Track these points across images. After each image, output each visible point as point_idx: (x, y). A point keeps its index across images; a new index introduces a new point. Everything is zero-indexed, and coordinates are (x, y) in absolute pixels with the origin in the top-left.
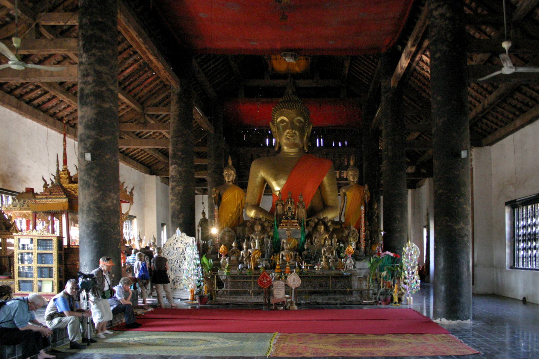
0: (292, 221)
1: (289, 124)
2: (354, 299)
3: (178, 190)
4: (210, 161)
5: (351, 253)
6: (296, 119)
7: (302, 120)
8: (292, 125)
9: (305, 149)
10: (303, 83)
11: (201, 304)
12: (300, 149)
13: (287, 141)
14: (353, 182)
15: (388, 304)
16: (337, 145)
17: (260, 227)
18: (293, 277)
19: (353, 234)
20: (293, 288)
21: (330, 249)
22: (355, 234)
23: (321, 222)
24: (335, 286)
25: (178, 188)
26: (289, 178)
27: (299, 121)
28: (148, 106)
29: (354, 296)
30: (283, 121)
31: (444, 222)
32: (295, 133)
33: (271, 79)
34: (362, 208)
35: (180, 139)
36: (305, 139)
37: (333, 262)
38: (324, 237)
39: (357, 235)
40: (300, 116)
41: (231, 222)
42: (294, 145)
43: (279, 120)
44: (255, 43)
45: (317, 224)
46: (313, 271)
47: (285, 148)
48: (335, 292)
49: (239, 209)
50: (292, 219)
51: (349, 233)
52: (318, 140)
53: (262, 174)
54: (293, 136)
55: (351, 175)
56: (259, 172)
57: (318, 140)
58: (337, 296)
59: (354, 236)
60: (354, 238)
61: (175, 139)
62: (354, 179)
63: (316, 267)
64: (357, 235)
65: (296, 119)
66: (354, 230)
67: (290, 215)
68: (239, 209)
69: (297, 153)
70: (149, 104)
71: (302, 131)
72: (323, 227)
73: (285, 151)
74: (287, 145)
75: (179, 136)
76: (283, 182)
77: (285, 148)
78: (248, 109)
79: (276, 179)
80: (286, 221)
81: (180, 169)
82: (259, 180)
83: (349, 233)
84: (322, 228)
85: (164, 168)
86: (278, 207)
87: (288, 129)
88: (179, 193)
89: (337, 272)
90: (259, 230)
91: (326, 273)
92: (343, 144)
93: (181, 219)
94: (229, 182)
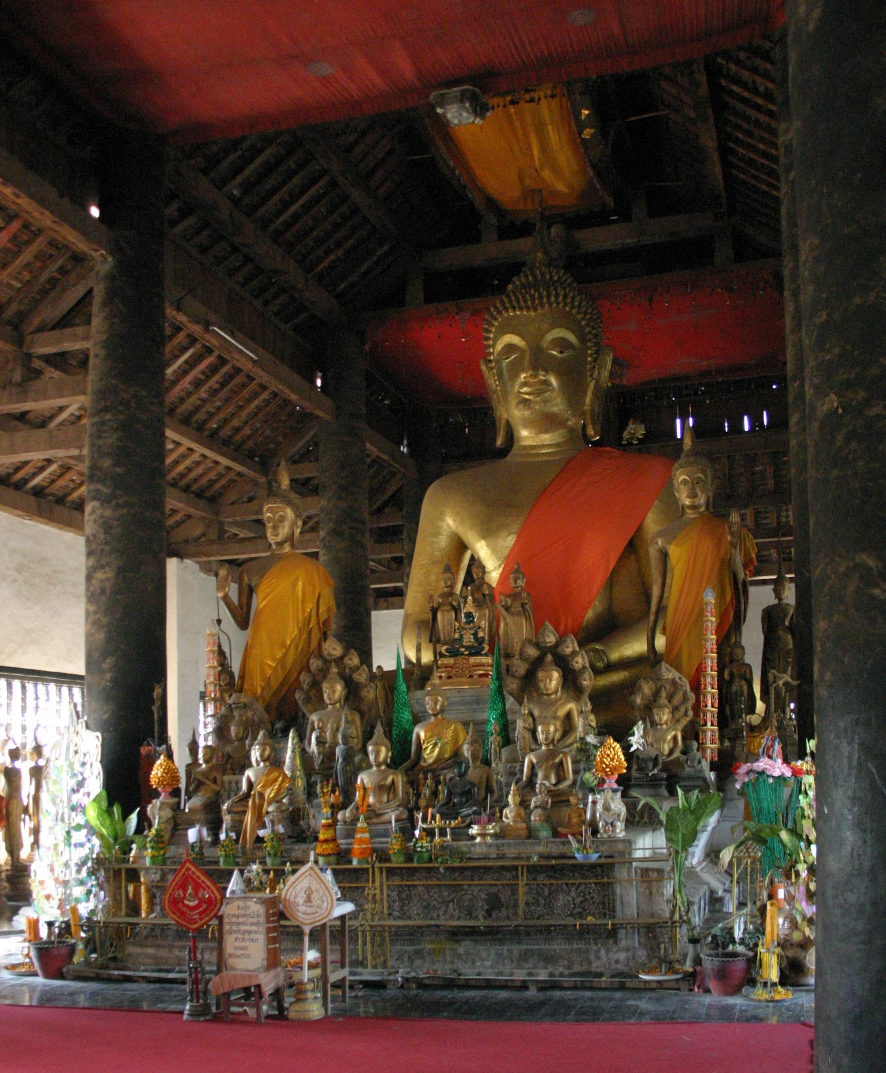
0: (473, 660)
1: (527, 357)
2: (622, 956)
3: (101, 581)
4: (324, 502)
5: (613, 769)
6: (549, 337)
7: (572, 338)
8: (538, 360)
9: (590, 431)
10: (599, 239)
11: (48, 975)
12: (571, 430)
13: (531, 420)
14: (694, 507)
15: (736, 991)
16: (737, 427)
17: (339, 688)
18: (304, 884)
19: (670, 698)
20: (307, 930)
21: (552, 754)
22: (679, 696)
23: (549, 658)
24: (550, 907)
25: (100, 575)
26: (524, 527)
27: (562, 344)
28: (40, 329)
29: (623, 943)
30: (510, 348)
31: (852, 586)
32: (546, 383)
33: (500, 238)
34: (710, 598)
35: (108, 417)
36: (588, 400)
37: (542, 806)
38: (562, 713)
39: (685, 699)
40: (561, 326)
41: (281, 675)
42: (548, 422)
43: (499, 346)
44: (326, 69)
45: (536, 665)
46: (463, 845)
47: (524, 433)
48: (547, 932)
49: (310, 633)
50: (471, 655)
51: (656, 694)
52: (678, 422)
53: (450, 523)
54: (538, 393)
55: (685, 482)
56: (441, 516)
57: (678, 422)
58: (558, 946)
59: (676, 702)
60: (675, 709)
61: (96, 419)
62: (693, 495)
63: (474, 830)
64: (685, 699)
65: (549, 337)
66: (673, 682)
67: (468, 639)
68: (310, 633)
69: (558, 445)
70: (36, 322)
71: (573, 376)
72: (556, 675)
73: (529, 442)
74: (527, 423)
75: (105, 410)
76: (508, 541)
77: (524, 433)
78: (430, 335)
79: (488, 532)
80: (451, 661)
81: (108, 513)
82: (443, 541)
83: (656, 694)
84: (553, 680)
85: (203, 535)
86: (439, 616)
87: (523, 371)
88: (103, 591)
89: (555, 849)
90: (337, 696)
91: (511, 852)
92: (756, 420)
93: (108, 676)
94: (280, 544)
